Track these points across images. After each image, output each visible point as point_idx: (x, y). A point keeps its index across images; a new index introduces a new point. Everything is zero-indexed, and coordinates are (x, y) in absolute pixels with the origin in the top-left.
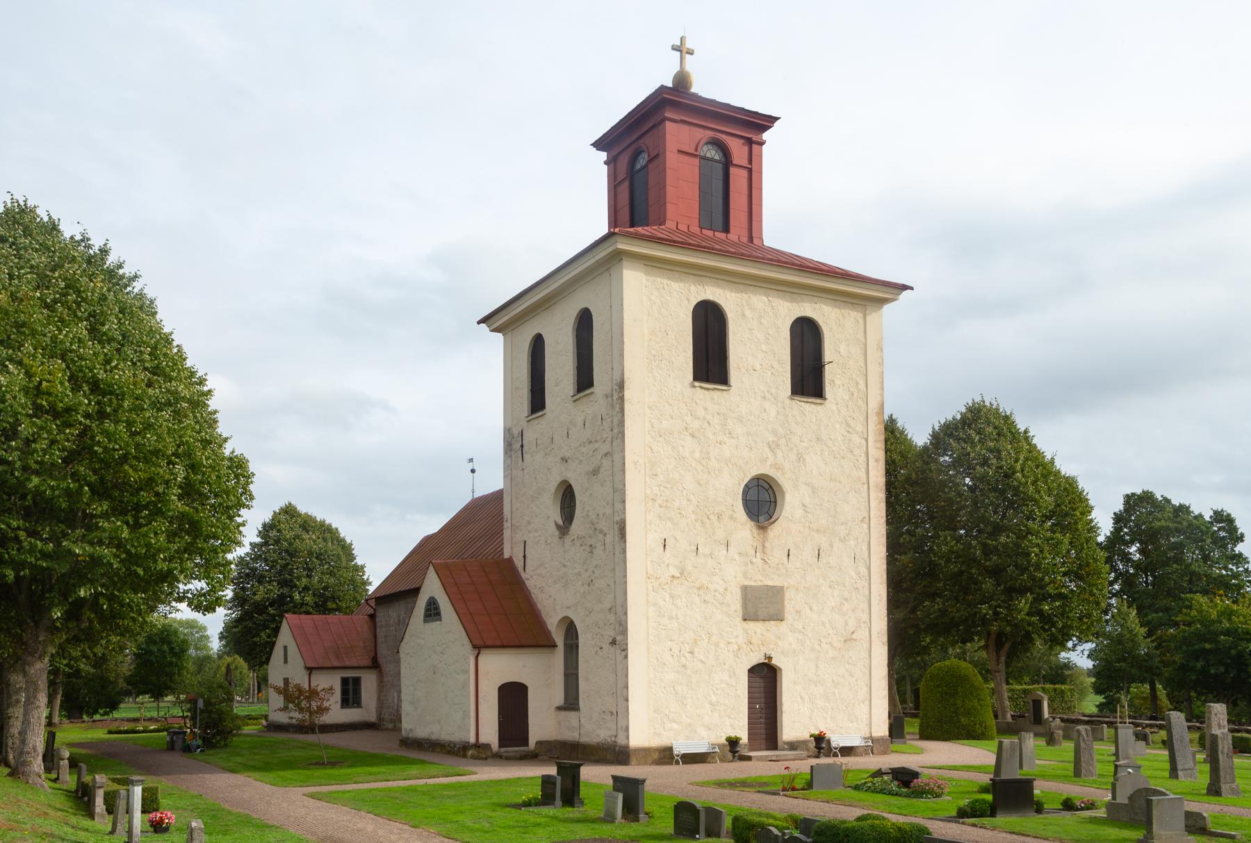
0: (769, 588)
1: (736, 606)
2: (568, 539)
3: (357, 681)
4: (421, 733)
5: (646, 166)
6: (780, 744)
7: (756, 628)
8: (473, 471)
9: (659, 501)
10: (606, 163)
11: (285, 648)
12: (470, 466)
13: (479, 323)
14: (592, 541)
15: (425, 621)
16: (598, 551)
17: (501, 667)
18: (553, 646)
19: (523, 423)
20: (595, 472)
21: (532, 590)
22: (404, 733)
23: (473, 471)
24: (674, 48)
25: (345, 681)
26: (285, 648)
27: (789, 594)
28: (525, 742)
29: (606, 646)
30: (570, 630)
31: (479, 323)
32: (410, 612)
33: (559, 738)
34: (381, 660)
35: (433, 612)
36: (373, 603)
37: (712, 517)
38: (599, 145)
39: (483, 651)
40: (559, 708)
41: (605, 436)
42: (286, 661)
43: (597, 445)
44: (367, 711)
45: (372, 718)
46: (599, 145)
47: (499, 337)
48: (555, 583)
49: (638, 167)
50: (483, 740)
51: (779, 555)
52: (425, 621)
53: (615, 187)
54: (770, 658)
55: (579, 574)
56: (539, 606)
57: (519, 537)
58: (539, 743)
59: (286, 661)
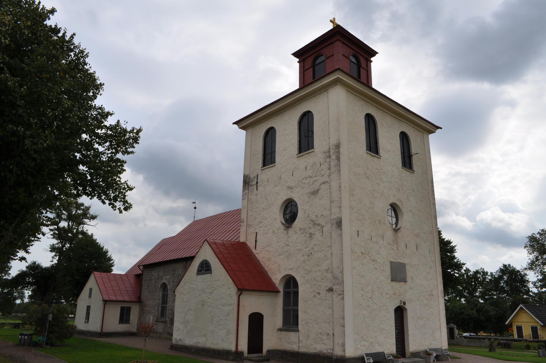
0: (400, 264)
1: (388, 272)
2: (291, 231)
3: (129, 309)
4: (189, 341)
5: (324, 61)
6: (408, 354)
7: (396, 285)
8: (195, 208)
9: (355, 210)
10: (298, 62)
11: (91, 290)
12: (194, 205)
13: (233, 124)
14: (312, 231)
15: (198, 274)
16: (318, 235)
17: (253, 303)
18: (278, 292)
19: (259, 172)
20: (315, 193)
21: (260, 260)
22: (174, 341)
23: (195, 208)
24: (331, 21)
25: (122, 309)
26: (91, 290)
27: (408, 268)
28: (261, 351)
29: (323, 293)
30: (291, 283)
31: (233, 124)
32: (186, 269)
33: (280, 348)
34: (143, 298)
35: (205, 268)
36: (142, 268)
37: (377, 222)
38: (296, 54)
39: (244, 293)
40: (280, 330)
41: (323, 173)
42: (90, 296)
43: (316, 178)
44: (132, 326)
45: (134, 330)
46: (296, 54)
47: (244, 132)
48: (280, 255)
49: (317, 62)
50: (240, 349)
51: (403, 246)
52: (198, 274)
53: (304, 72)
54: (405, 303)
55: (300, 250)
56: (266, 269)
57: (251, 230)
58: (268, 351)
59: (90, 296)
